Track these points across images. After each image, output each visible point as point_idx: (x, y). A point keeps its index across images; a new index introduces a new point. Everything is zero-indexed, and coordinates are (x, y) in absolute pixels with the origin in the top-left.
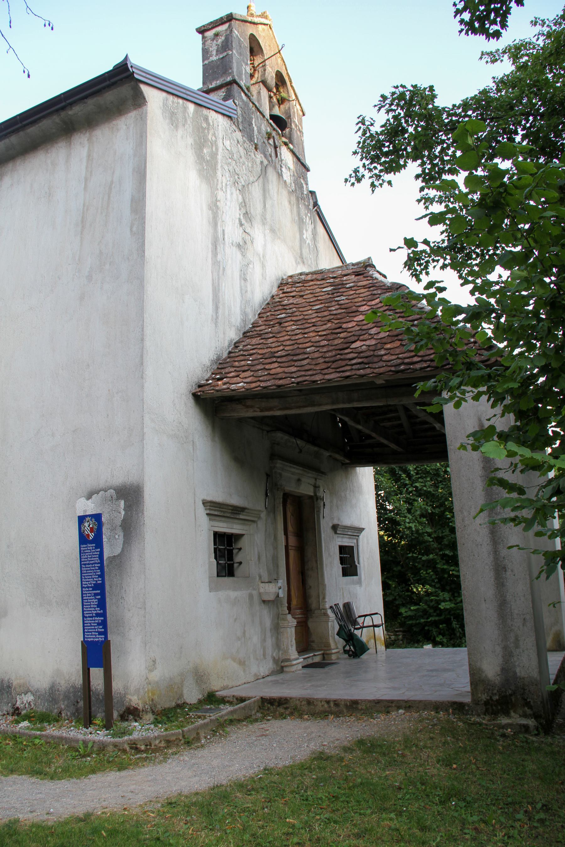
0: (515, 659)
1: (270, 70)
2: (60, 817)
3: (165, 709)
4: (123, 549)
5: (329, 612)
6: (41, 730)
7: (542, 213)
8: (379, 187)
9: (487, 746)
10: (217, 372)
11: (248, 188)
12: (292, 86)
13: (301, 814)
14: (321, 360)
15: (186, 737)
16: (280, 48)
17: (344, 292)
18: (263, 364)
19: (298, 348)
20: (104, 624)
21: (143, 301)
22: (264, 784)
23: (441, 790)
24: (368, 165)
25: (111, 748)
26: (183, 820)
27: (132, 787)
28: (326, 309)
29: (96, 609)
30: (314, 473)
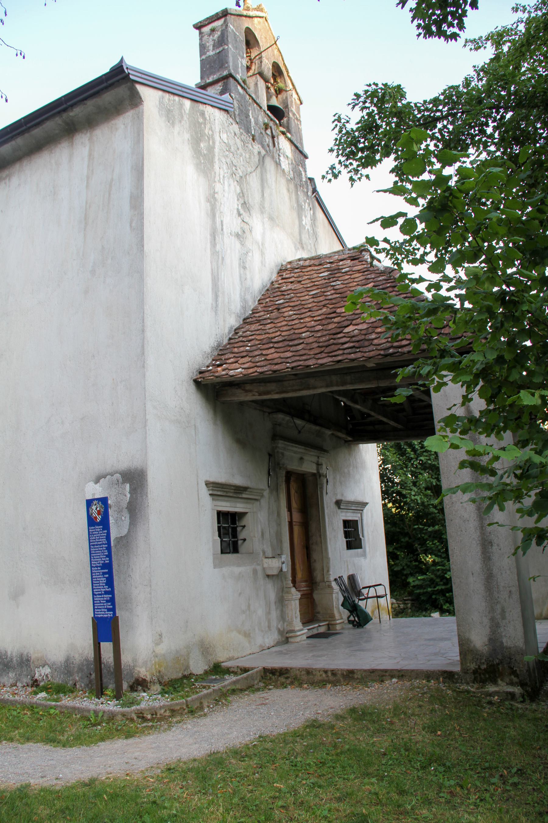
0: (502, 630)
1: (267, 62)
2: (68, 782)
3: (172, 680)
4: (129, 530)
5: (334, 584)
6: (56, 700)
7: (487, 214)
8: (358, 180)
9: (472, 713)
10: (217, 358)
11: (246, 179)
12: (289, 76)
13: (289, 779)
14: (315, 345)
15: (190, 706)
16: (276, 39)
17: (339, 277)
18: (261, 350)
19: (294, 333)
20: (112, 601)
21: (143, 294)
22: (257, 751)
23: (423, 755)
24: (344, 161)
25: (119, 717)
26: (179, 784)
27: (137, 754)
28: (322, 294)
29: (105, 587)
30: (316, 451)
